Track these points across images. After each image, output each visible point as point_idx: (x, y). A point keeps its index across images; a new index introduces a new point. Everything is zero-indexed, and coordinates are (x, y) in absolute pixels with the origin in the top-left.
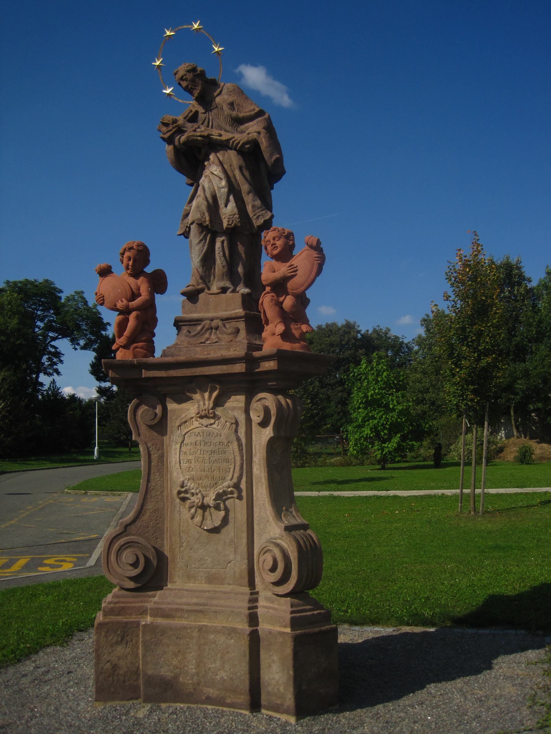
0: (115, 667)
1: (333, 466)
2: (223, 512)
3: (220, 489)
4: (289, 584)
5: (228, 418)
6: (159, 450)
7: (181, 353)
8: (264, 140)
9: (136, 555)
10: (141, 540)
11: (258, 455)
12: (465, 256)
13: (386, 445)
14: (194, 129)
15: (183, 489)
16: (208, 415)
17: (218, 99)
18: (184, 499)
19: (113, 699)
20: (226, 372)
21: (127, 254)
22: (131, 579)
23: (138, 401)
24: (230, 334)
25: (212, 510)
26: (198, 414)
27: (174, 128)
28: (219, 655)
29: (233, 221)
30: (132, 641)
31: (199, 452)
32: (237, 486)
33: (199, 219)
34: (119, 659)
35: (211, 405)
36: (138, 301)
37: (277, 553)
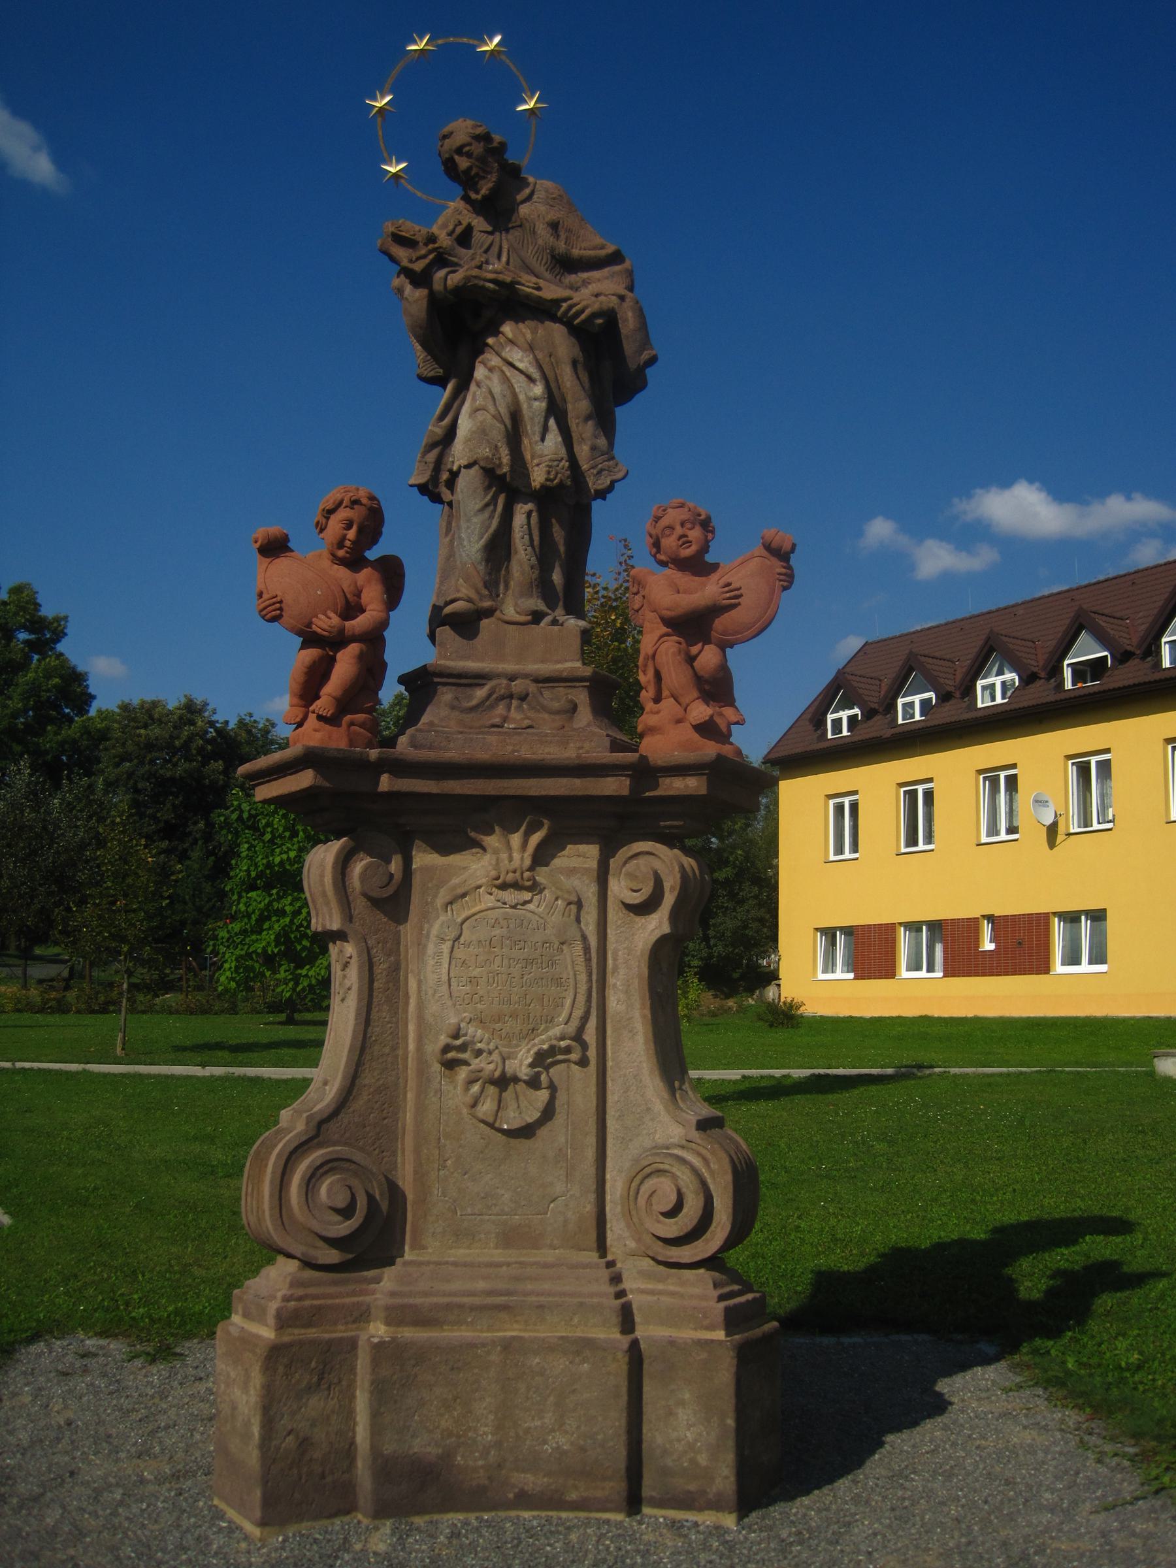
0: (305, 1443)
1: (171, 1013)
2: (544, 1091)
3: (543, 1042)
4: (707, 1241)
5: (561, 890)
6: (389, 955)
7: (452, 745)
8: (630, 314)
9: (350, 1188)
10: (358, 1156)
11: (622, 972)
12: (605, 589)
13: (304, 972)
14: (476, 262)
15: (458, 1042)
16: (520, 882)
17: (524, 210)
18: (451, 1066)
19: (300, 1518)
20: (580, 793)
21: (343, 514)
22: (333, 1242)
23: (352, 844)
24: (558, 712)
25: (521, 1087)
26: (498, 878)
27: (430, 252)
28: (552, 1398)
29: (557, 473)
30: (340, 1381)
31: (498, 961)
32: (578, 1037)
33: (487, 458)
34: (313, 1425)
35: (528, 862)
36: (360, 623)
37: (685, 1178)
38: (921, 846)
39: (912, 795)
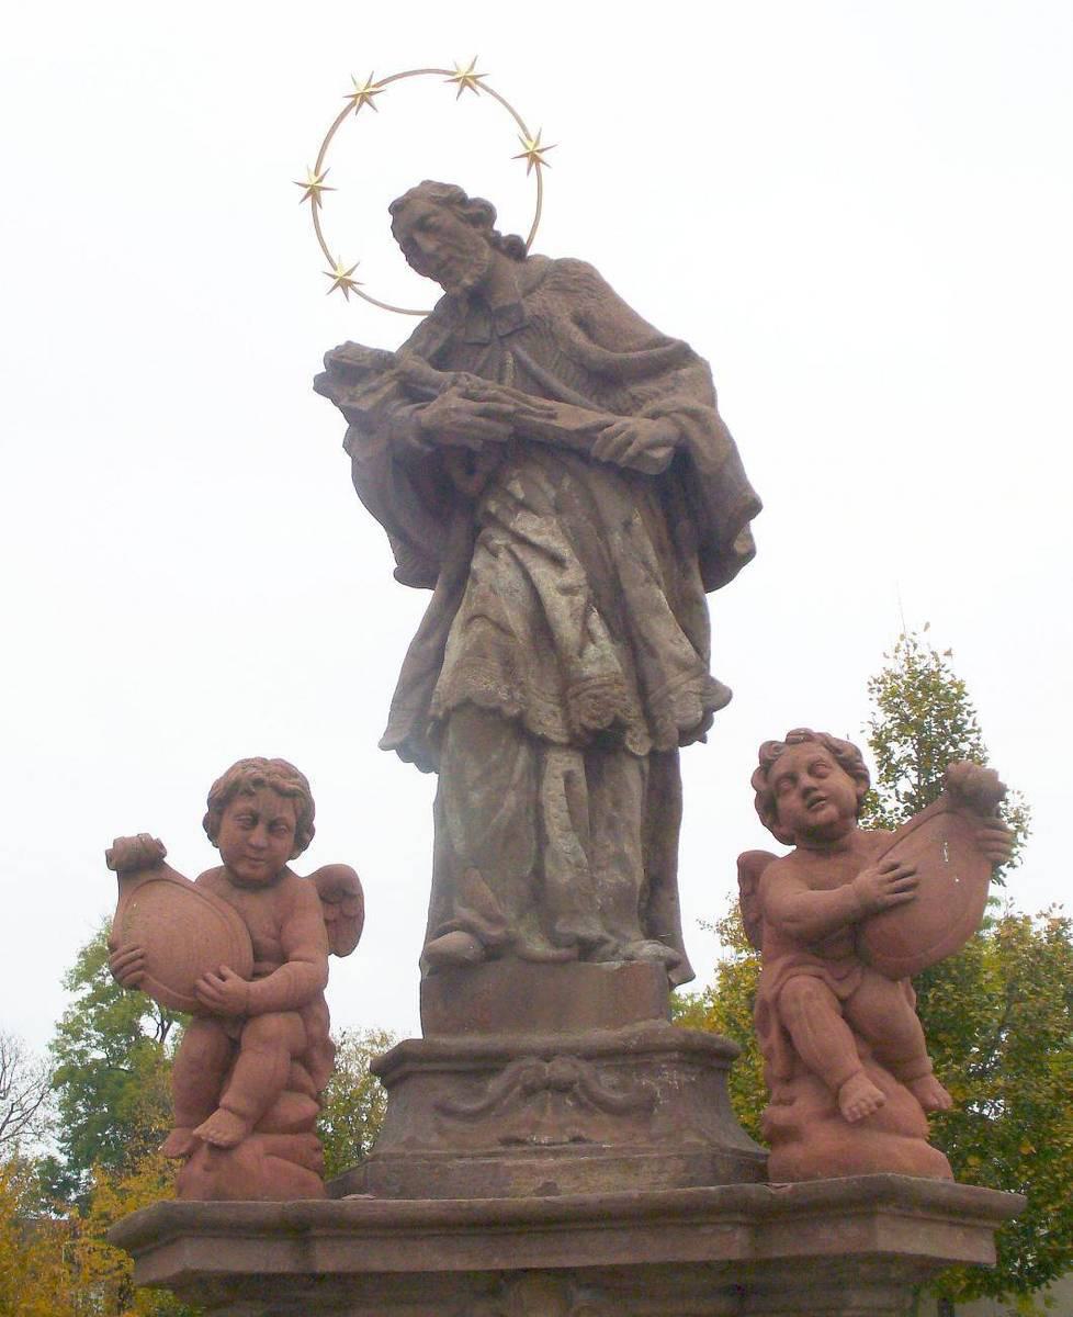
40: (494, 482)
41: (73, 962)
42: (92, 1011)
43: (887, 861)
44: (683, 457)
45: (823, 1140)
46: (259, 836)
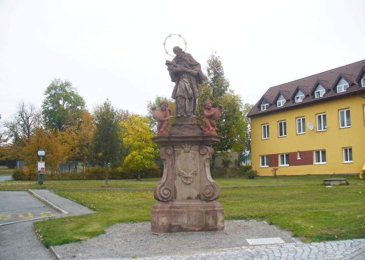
38: (284, 136)
39: (281, 124)
40: (182, 75)
41: (45, 89)
42: (50, 99)
43: (214, 111)
44: (198, 74)
45: (208, 132)
46: (165, 107)
